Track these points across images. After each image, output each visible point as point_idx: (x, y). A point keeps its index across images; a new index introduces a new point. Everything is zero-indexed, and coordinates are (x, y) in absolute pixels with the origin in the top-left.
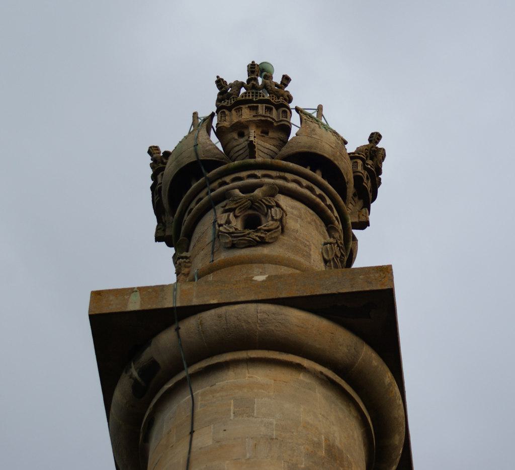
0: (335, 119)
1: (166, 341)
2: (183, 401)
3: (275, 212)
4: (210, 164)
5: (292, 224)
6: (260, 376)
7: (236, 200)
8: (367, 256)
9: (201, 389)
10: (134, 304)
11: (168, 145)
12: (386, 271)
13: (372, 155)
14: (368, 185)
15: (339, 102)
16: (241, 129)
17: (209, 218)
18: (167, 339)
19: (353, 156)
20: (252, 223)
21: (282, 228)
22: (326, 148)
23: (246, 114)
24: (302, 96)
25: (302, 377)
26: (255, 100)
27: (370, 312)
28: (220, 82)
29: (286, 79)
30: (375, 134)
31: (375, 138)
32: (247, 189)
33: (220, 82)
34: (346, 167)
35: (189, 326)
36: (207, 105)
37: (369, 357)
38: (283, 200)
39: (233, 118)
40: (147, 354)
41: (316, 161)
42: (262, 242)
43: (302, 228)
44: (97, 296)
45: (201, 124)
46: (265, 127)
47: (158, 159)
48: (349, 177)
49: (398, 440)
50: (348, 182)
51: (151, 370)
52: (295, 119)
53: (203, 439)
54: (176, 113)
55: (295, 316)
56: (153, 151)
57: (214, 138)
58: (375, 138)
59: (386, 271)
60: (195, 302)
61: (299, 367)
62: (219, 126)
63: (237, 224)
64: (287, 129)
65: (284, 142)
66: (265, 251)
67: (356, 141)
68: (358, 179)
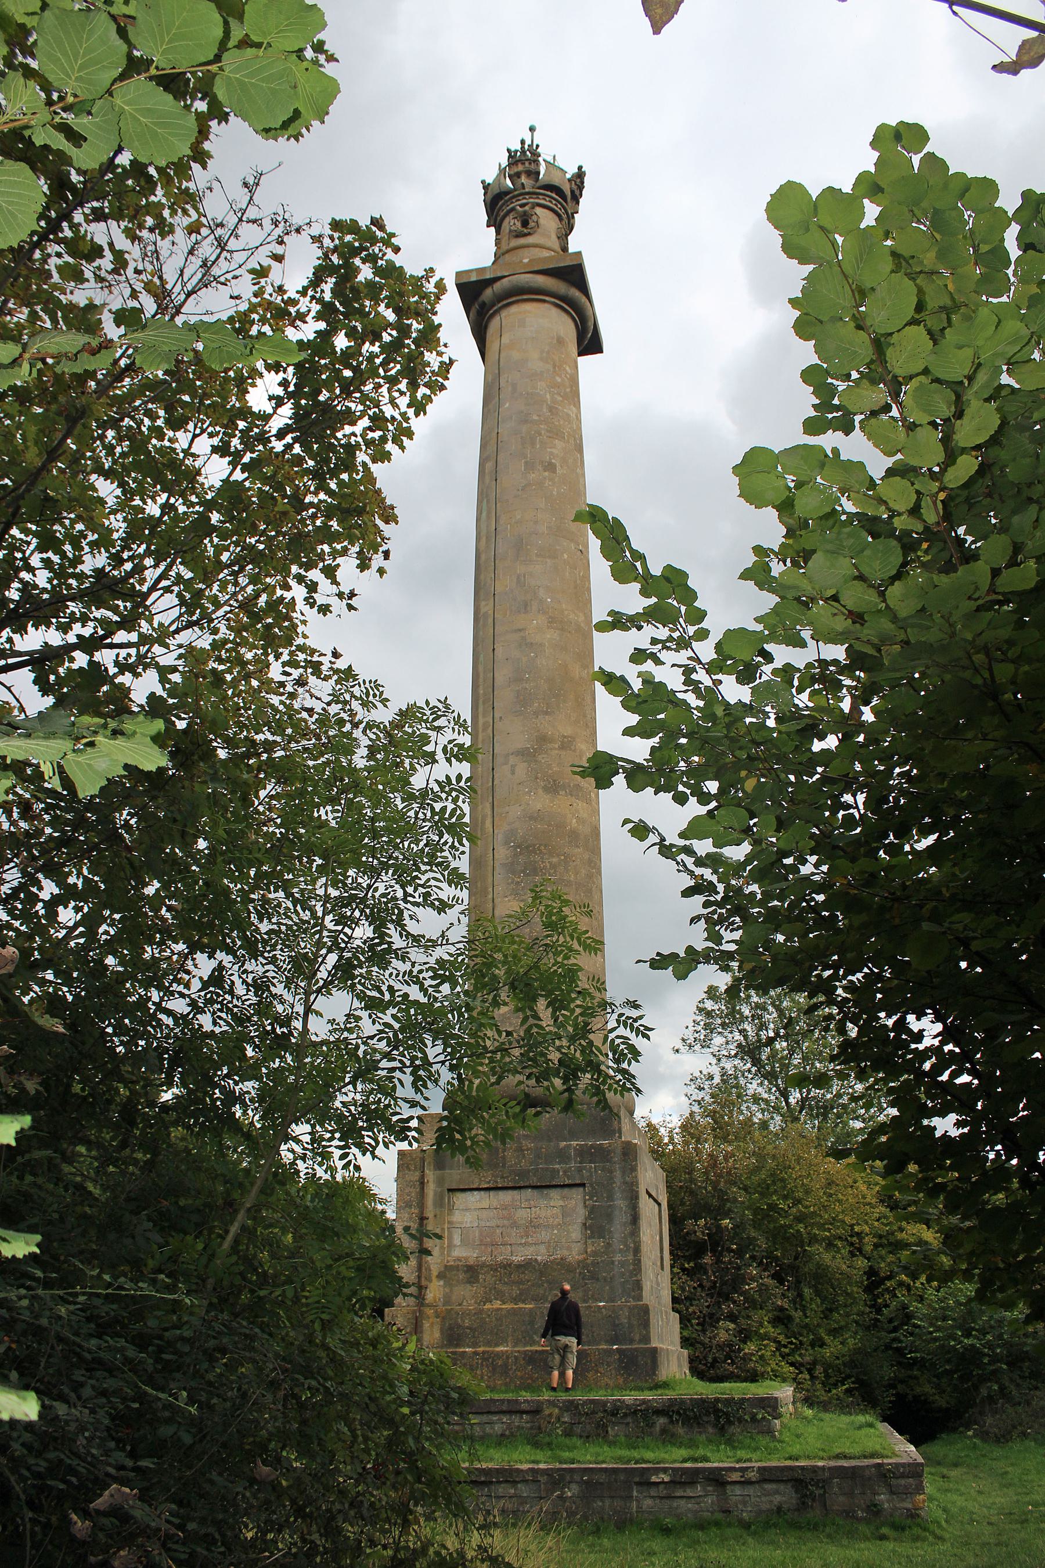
0: (560, 163)
1: (488, 293)
3: (534, 218)
4: (508, 192)
5: (541, 221)
7: (518, 212)
8: (574, 243)
9: (504, 313)
10: (474, 278)
11: (489, 180)
12: (580, 253)
13: (580, 175)
14: (577, 193)
15: (561, 154)
16: (518, 175)
17: (507, 220)
19: (569, 180)
20: (525, 224)
22: (556, 181)
23: (520, 168)
24: (546, 153)
25: (546, 305)
26: (523, 160)
27: (574, 274)
28: (509, 150)
31: (580, 168)
32: (522, 206)
33: (509, 150)
34: (566, 189)
35: (497, 286)
36: (505, 163)
37: (575, 293)
38: (539, 211)
39: (515, 169)
42: (529, 234)
43: (546, 220)
44: (458, 274)
45: (502, 171)
46: (529, 173)
47: (486, 187)
48: (568, 194)
50: (566, 195)
51: (483, 305)
53: (505, 339)
54: (490, 166)
56: (483, 182)
57: (508, 182)
59: (580, 253)
60: (499, 274)
61: (544, 301)
63: (519, 224)
64: (538, 173)
65: (537, 180)
66: (530, 240)
67: (571, 171)
68: (572, 192)
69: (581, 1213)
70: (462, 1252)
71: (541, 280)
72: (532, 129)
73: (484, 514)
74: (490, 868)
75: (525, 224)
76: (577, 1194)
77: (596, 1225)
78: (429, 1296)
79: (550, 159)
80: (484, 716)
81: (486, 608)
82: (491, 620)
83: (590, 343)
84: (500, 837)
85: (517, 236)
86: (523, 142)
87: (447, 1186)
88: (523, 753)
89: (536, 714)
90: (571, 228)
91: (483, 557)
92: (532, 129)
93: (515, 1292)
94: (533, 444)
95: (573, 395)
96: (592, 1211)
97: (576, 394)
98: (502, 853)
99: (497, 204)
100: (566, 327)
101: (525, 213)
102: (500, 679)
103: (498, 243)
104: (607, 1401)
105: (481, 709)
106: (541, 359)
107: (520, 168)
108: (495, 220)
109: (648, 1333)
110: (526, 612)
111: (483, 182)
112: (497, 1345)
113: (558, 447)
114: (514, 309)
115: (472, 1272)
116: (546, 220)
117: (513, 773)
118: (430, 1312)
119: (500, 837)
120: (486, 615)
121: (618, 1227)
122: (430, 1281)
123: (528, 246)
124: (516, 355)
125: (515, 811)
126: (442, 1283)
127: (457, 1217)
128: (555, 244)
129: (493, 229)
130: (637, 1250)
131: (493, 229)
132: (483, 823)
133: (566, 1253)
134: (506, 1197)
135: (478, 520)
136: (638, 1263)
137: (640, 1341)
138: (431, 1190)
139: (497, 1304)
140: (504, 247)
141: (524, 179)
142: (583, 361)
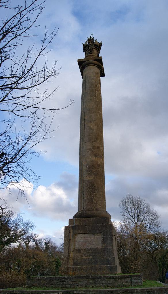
0: (97, 41)
2: (85, 69)
4: (88, 45)
5: (94, 51)
6: (91, 66)
8: (100, 55)
9: (87, 68)
10: (81, 61)
11: (84, 43)
12: (101, 57)
13: (101, 43)
15: (98, 39)
16: (90, 42)
18: (84, 63)
20: (91, 51)
21: (93, 52)
22: (97, 44)
23: (90, 41)
24: (95, 39)
26: (91, 40)
27: (100, 60)
29: (93, 37)
30: (101, 135)
31: (101, 42)
34: (99, 45)
35: (86, 62)
36: (87, 40)
37: (100, 64)
38: (93, 49)
40: (83, 65)
41: (96, 45)
42: (92, 53)
43: (95, 51)
45: (86, 42)
46: (92, 42)
47: (83, 45)
49: (103, 70)
50: (99, 46)
51: (83, 66)
52: (94, 41)
53: (87, 72)
55: (94, 61)
56: (83, 44)
57: (88, 44)
58: (101, 42)
62: (3, 246)
63: (90, 52)
66: (92, 54)
67: (99, 42)
68: (100, 46)
69: (101, 239)
70: (77, 247)
71: (94, 61)
72: (92, 35)
73: (83, 105)
74: (83, 171)
75: (91, 51)
76: (100, 235)
77: (104, 242)
78: (71, 256)
79: (96, 40)
80: (82, 142)
81: (83, 122)
82: (84, 124)
83: (103, 75)
84: (85, 165)
85: (89, 54)
86: (91, 36)
87: (74, 233)
88: (90, 149)
89: (92, 142)
90: (99, 53)
91: (82, 113)
92: (92, 35)
93: (88, 255)
94: (92, 92)
95: (100, 83)
96: (104, 238)
97: (100, 83)
98: (86, 168)
99: (86, 48)
100: (97, 70)
101: (91, 50)
102: (85, 135)
103: (85, 55)
104: (108, 276)
105: (82, 141)
106: (94, 76)
107: (90, 41)
108: (85, 51)
109: (115, 263)
110: (91, 123)
111: (83, 44)
112: (84, 265)
113: (87, 178)
114: (89, 67)
115: (79, 251)
116: (95, 51)
117: (88, 153)
118: (71, 259)
119: (85, 165)
120: (83, 124)
121: (109, 242)
122: (71, 252)
123: (91, 55)
124: (89, 75)
125: (88, 160)
126: (73, 253)
127: (76, 239)
128: (96, 55)
129: (84, 53)
130: (113, 246)
131: (84, 53)
132: (82, 162)
133: (98, 246)
134: (87, 235)
135: (81, 106)
136: (113, 248)
137: (113, 264)
138: (71, 234)
139: (84, 257)
140: (87, 56)
141: (91, 43)
142: (101, 78)
